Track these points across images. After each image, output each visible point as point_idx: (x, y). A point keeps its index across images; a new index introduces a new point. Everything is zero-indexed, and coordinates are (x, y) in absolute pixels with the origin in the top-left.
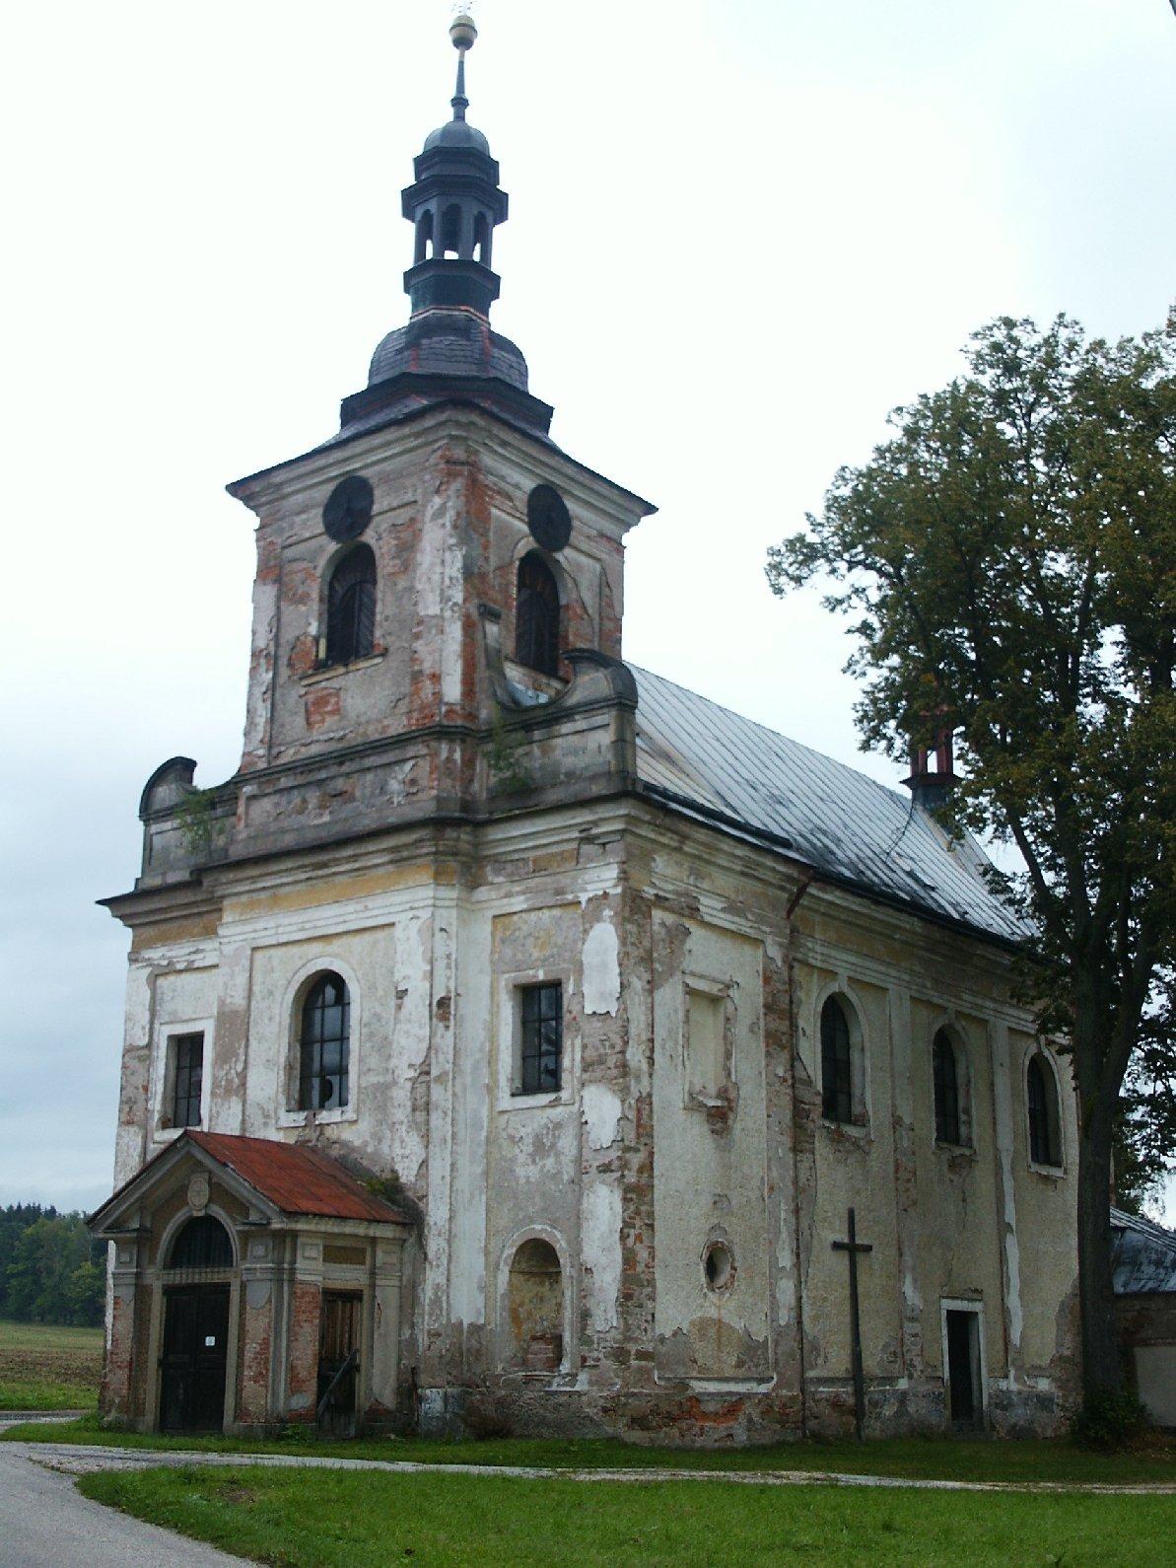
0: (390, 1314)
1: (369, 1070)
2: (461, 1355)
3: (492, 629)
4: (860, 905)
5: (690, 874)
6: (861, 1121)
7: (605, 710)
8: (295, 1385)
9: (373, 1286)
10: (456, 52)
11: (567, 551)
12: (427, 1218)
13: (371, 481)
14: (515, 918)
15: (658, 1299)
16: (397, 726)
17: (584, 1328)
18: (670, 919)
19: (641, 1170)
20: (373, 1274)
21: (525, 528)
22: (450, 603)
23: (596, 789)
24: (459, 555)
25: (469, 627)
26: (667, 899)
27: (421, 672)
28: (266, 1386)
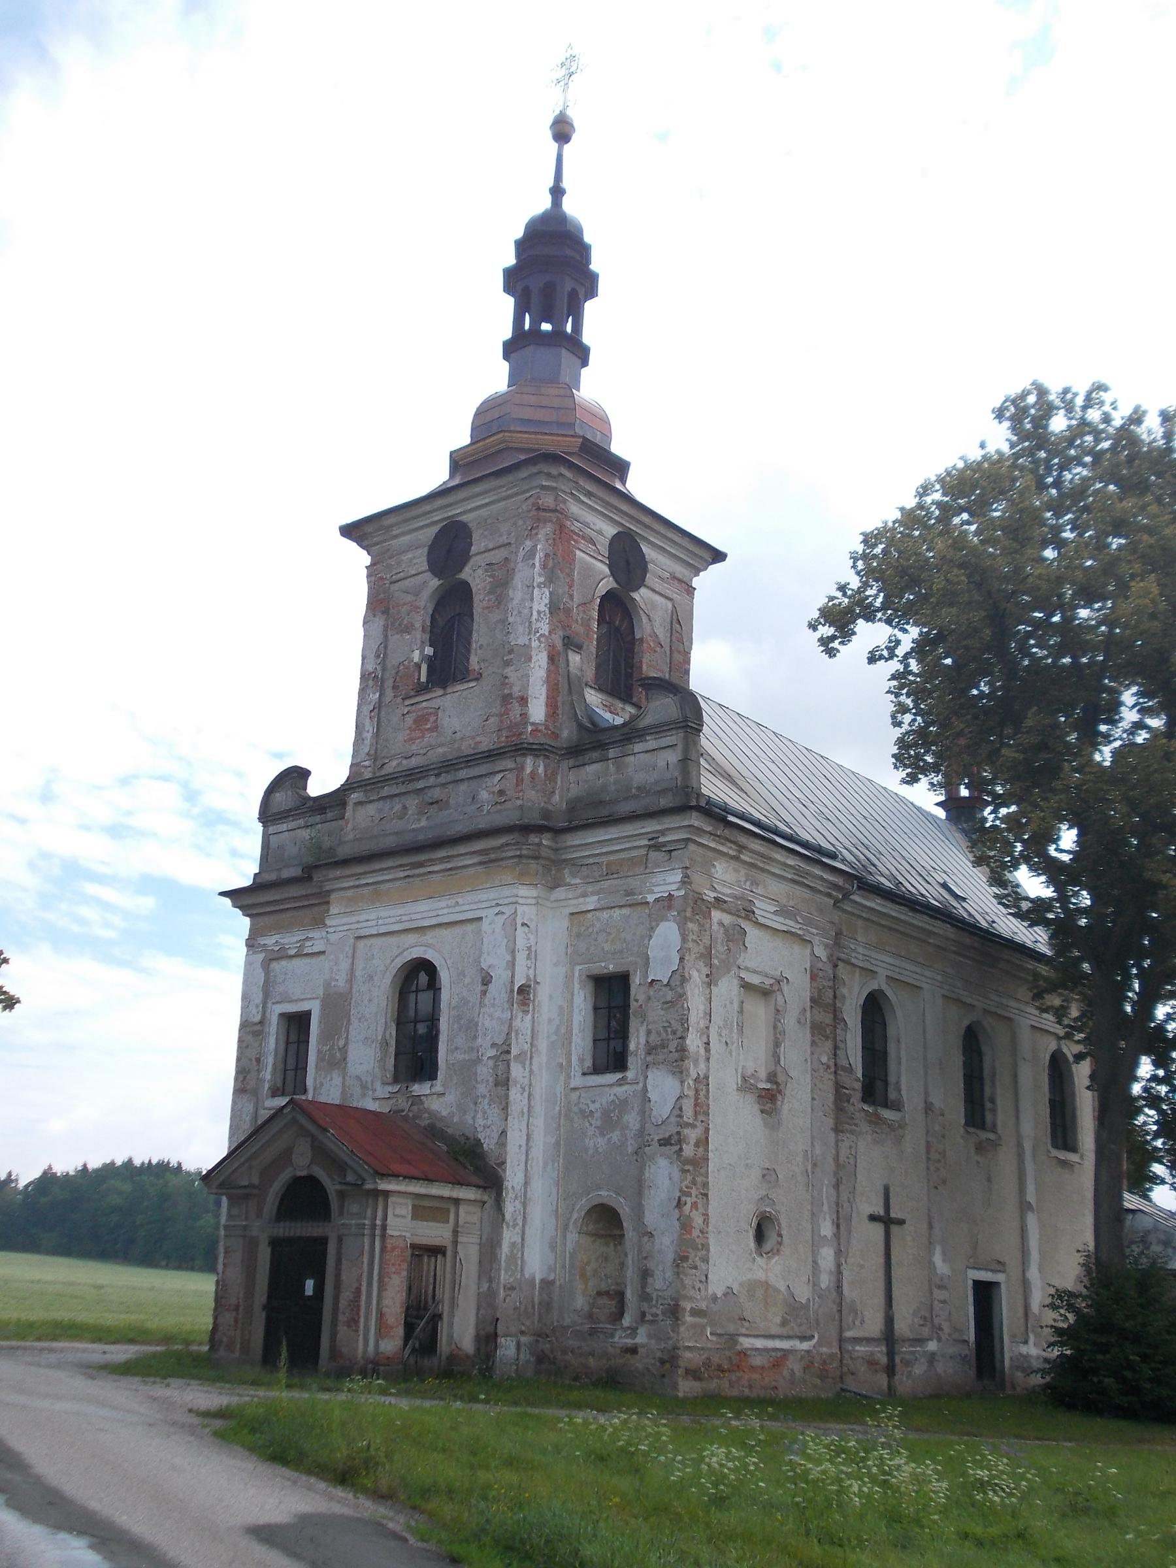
2: (533, 1307)
6: (897, 1106)
7: (674, 732)
9: (455, 1243)
10: (556, 145)
12: (506, 1183)
13: (470, 525)
14: (589, 915)
16: (486, 743)
17: (644, 1287)
18: (727, 919)
19: (697, 1145)
20: (456, 1232)
21: (607, 570)
22: (538, 635)
23: (665, 802)
26: (725, 902)
28: (357, 1331)
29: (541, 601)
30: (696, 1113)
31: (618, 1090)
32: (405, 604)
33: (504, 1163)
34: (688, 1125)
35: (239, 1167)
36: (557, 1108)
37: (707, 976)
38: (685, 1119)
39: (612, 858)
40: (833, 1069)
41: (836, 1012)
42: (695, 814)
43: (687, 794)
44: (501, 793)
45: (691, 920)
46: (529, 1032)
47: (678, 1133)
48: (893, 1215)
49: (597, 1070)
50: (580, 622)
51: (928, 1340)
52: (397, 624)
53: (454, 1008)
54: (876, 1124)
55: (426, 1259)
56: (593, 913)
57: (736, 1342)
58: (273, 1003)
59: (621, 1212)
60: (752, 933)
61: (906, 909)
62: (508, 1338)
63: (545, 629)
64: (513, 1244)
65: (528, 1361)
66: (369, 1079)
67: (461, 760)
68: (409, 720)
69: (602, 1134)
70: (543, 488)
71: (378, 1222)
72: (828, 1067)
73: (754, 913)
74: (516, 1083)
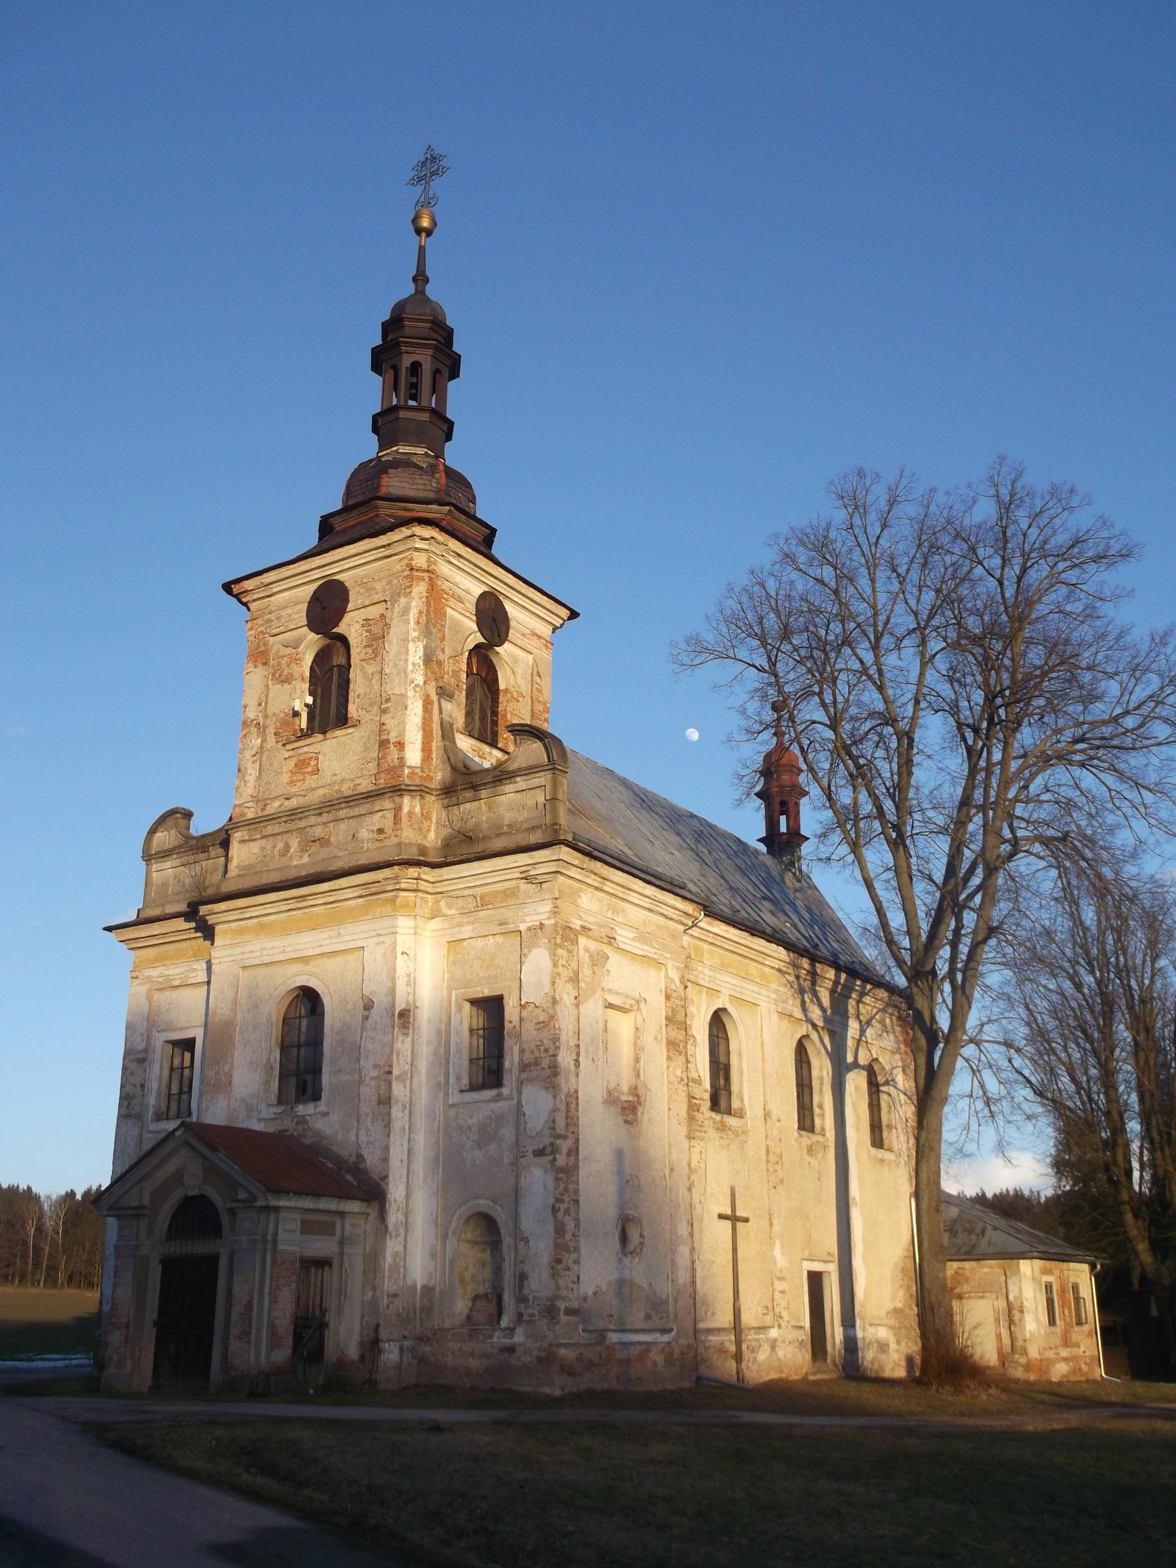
0: (356, 1279)
1: (340, 1070)
2: (415, 1312)
3: (447, 706)
4: (739, 937)
5: (609, 909)
6: (741, 1114)
7: (542, 774)
8: (275, 1341)
9: (342, 1254)
11: (507, 645)
12: (389, 1196)
13: (347, 584)
14: (465, 943)
15: (582, 1264)
16: (365, 785)
17: (521, 1288)
18: (593, 945)
19: (569, 1154)
20: (342, 1243)
21: (475, 627)
22: (413, 685)
23: (534, 838)
24: (421, 645)
25: (427, 703)
26: (590, 930)
27: (388, 741)
28: (249, 1343)
29: (416, 653)
30: (567, 1125)
31: (495, 1106)
32: (284, 656)
33: (386, 1177)
34: (559, 1137)
35: (130, 1189)
36: (436, 1124)
37: (576, 998)
38: (558, 1131)
39: (485, 889)
40: (686, 1081)
41: (684, 1027)
42: (565, 849)
43: (556, 831)
44: (380, 831)
45: (561, 946)
46: (409, 1053)
47: (552, 1144)
48: (738, 1214)
49: (474, 1087)
50: (451, 674)
51: (770, 1327)
52: (277, 675)
53: (337, 1033)
54: (723, 1130)
55: (313, 1270)
56: (469, 941)
57: (604, 1338)
58: (158, 1032)
59: (498, 1219)
60: (614, 958)
61: (746, 934)
62: (391, 1343)
63: (420, 680)
64: (396, 1254)
65: (410, 1364)
66: (254, 1102)
67: (342, 801)
68: (291, 764)
69: (480, 1148)
70: (417, 550)
71: (269, 1237)
72: (682, 1079)
73: (615, 939)
74: (397, 1101)
